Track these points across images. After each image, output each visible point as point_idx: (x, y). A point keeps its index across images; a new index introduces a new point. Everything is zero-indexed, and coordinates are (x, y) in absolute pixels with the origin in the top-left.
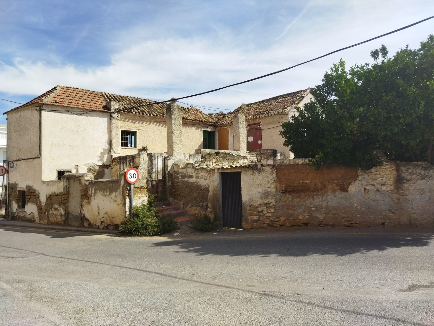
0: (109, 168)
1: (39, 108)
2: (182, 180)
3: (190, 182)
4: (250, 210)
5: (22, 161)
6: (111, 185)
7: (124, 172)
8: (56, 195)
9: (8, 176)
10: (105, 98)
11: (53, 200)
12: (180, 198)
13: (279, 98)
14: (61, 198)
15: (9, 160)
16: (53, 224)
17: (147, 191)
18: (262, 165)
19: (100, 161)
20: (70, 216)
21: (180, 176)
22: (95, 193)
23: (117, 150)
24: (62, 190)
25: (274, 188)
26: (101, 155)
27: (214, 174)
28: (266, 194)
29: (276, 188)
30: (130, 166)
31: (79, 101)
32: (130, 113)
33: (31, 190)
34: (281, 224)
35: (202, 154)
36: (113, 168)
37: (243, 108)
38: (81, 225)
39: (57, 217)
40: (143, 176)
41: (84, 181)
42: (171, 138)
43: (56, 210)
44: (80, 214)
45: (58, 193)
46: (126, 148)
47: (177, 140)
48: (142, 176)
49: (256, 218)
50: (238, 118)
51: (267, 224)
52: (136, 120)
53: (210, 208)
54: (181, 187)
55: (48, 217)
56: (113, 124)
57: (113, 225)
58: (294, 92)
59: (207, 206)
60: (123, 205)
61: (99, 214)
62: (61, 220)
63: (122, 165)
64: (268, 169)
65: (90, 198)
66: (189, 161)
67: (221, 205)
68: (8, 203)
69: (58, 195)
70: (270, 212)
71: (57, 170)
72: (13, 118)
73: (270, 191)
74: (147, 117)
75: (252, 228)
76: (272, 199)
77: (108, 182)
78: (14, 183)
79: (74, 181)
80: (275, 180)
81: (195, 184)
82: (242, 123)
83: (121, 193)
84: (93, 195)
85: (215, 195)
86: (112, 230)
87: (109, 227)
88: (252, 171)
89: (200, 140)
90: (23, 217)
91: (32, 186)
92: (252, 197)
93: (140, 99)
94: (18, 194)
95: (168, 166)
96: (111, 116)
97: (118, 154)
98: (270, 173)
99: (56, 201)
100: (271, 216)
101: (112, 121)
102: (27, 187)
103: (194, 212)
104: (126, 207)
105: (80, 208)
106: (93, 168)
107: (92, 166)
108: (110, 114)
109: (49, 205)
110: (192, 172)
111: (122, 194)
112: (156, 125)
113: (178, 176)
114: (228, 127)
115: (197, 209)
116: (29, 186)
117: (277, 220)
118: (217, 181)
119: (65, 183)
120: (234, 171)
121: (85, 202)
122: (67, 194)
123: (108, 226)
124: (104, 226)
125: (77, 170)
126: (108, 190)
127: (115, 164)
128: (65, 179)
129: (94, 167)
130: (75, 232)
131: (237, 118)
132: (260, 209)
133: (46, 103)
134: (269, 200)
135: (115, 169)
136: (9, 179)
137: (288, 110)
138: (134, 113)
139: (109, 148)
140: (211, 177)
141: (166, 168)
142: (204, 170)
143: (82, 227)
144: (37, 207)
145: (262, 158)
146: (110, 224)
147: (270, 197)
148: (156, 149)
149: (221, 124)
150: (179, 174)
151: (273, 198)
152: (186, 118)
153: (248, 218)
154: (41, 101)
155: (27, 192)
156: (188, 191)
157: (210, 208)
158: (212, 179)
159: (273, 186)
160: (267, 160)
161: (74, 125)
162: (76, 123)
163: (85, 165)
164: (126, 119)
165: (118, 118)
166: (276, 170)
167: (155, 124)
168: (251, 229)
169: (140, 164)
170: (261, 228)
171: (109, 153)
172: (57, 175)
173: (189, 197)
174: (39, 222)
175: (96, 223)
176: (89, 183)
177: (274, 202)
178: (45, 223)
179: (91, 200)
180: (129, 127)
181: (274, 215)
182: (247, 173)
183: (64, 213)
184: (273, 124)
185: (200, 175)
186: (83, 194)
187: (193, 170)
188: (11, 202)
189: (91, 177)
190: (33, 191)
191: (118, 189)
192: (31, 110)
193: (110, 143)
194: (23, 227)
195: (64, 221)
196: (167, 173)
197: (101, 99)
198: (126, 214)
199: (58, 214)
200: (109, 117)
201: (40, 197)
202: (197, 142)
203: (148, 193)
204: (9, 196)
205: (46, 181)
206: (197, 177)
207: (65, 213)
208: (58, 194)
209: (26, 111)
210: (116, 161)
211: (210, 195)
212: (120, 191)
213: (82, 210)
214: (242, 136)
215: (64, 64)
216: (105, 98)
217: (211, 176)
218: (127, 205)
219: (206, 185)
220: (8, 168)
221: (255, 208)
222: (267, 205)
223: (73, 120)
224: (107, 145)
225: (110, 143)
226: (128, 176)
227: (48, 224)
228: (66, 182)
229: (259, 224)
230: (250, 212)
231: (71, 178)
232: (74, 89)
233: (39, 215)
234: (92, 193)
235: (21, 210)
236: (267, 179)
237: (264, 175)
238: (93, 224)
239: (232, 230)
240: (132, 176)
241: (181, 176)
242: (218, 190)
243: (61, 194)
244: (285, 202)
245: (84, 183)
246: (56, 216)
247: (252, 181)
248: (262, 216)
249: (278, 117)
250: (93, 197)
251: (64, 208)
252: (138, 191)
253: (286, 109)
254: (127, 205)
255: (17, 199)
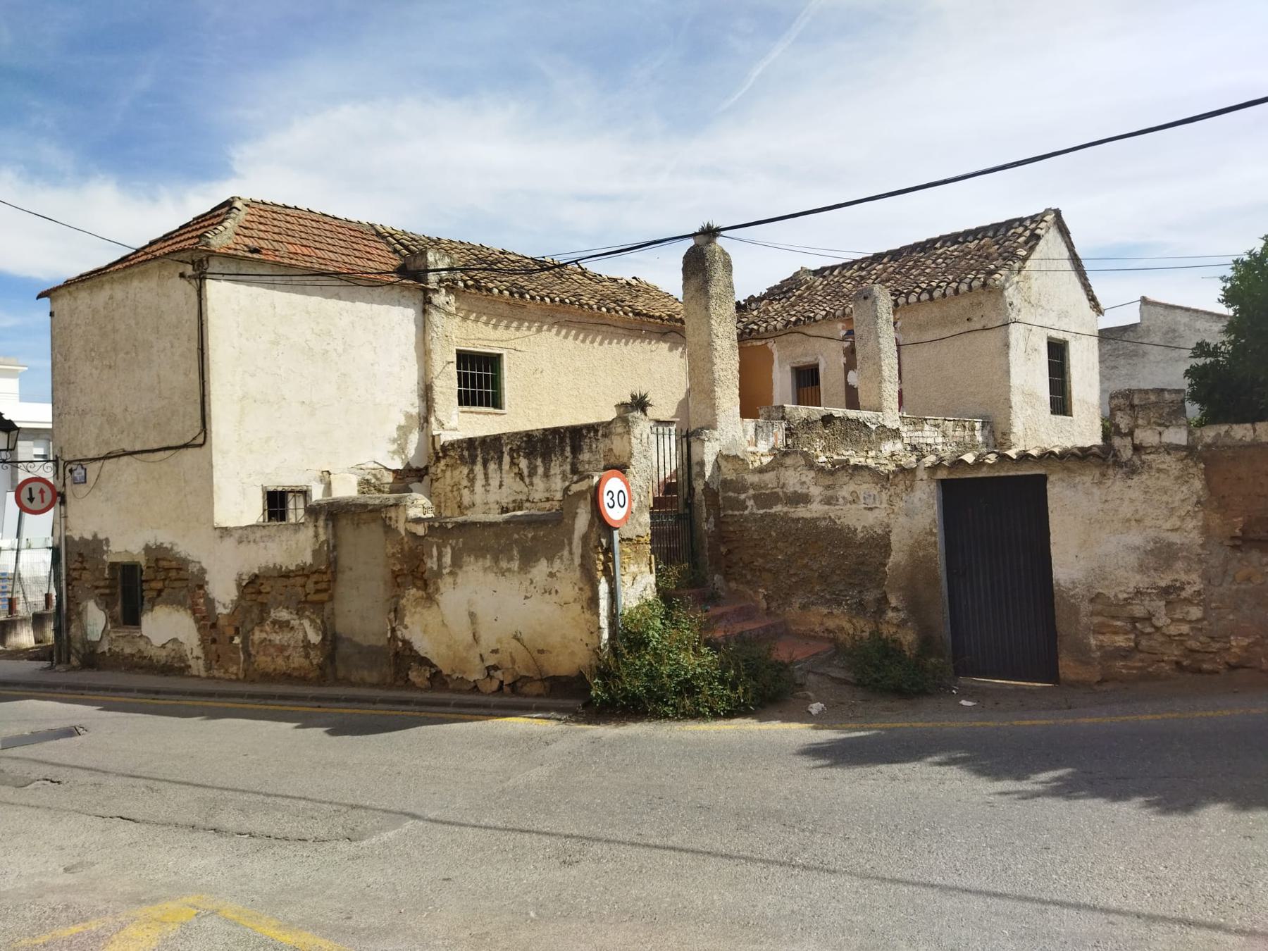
0: (426, 477)
1: (194, 270)
2: (761, 512)
3: (798, 520)
4: (1093, 614)
5: (125, 459)
6: (530, 535)
7: (590, 487)
8: (282, 576)
9: (66, 512)
10: (389, 243)
11: (268, 593)
12: (749, 577)
13: (938, 245)
14: (304, 586)
15: (67, 458)
16: (267, 677)
17: (653, 552)
18: (1137, 449)
19: (396, 457)
20: (343, 649)
21: (750, 499)
22: (457, 563)
23: (449, 417)
24: (308, 559)
25: (1196, 532)
26: (399, 435)
27: (910, 488)
28: (1163, 554)
29: (1206, 530)
30: (517, 471)
31: (317, 251)
32: (485, 293)
33: (164, 559)
34: (1233, 661)
35: (788, 421)
36: (437, 480)
37: (807, 282)
38: (396, 680)
39: (286, 654)
40: (642, 498)
41: (407, 521)
42: (709, 365)
43: (280, 627)
44: (389, 640)
45: (293, 568)
46: (472, 412)
47: (725, 373)
48: (637, 497)
49: (1123, 644)
50: (874, 302)
51: (1172, 661)
52: (501, 317)
53: (895, 609)
54: (755, 537)
55: (248, 655)
56: (435, 329)
57: (541, 680)
58: (992, 225)
59: (883, 601)
60: (589, 605)
61: (476, 638)
62: (308, 662)
63: (478, 468)
64: (1170, 462)
65: (435, 583)
66: (756, 446)
67: (947, 598)
68: (68, 609)
69: (292, 574)
70: (1183, 620)
71: (264, 488)
72: (81, 308)
73: (1178, 542)
74: (531, 306)
75: (1106, 681)
76: (1187, 572)
77: (514, 522)
78: (88, 536)
79: (358, 524)
80: (1198, 502)
81: (823, 523)
82: (884, 317)
83: (577, 561)
84: (445, 571)
85: (918, 564)
86: (538, 696)
87: (522, 687)
88: (1097, 473)
89: (680, 383)
90: (133, 655)
91: (169, 546)
92: (1101, 568)
93: (488, 249)
94: (106, 575)
95: (702, 464)
96: (428, 301)
97: (452, 432)
98: (1177, 478)
99: (282, 598)
100: (1188, 635)
101: (430, 317)
102: (147, 549)
103: (822, 624)
104: (601, 611)
105: (390, 620)
106: (378, 479)
107: (373, 472)
108: (422, 293)
109: (248, 611)
110: (804, 483)
111: (582, 565)
112: (558, 333)
113: (743, 496)
114: (772, 340)
115: (835, 611)
116: (160, 547)
117: (1215, 646)
118: (930, 512)
119: (321, 531)
120: (1012, 473)
121: (411, 597)
122: (329, 571)
123: (519, 684)
124: (502, 682)
125: (328, 487)
126: (515, 553)
127: (447, 466)
128: (322, 518)
129: (379, 476)
130: (390, 707)
131: (869, 301)
132: (1138, 611)
133: (222, 251)
134: (1176, 577)
135: (448, 481)
136: (69, 524)
137: (1003, 277)
138: (496, 291)
139: (424, 411)
140: (896, 500)
141: (695, 469)
142: (863, 473)
143: (400, 688)
144: (197, 621)
145: (1140, 422)
146: (527, 675)
147: (1179, 565)
148: (561, 414)
149: (748, 331)
150: (744, 489)
151: (1195, 566)
152: (645, 312)
153: (1089, 644)
154: (203, 243)
155: (148, 567)
156: (790, 551)
157: (895, 609)
158: (902, 504)
159: (1190, 524)
160: (1160, 429)
161: (313, 329)
162: (318, 323)
163: (351, 470)
164: (470, 311)
165: (449, 308)
166: (1202, 466)
167: (554, 330)
168: (1099, 683)
169: (631, 455)
170: (1145, 677)
171: (422, 429)
172: (264, 506)
173: (792, 572)
174: (203, 674)
175: (465, 672)
176: (431, 528)
177: (1198, 580)
178: (233, 677)
179: (437, 589)
180: (479, 339)
181: (1200, 630)
182: (1077, 480)
183: (320, 638)
184: (945, 327)
185: (845, 492)
186: (401, 570)
187: (812, 474)
188: (78, 604)
189: (425, 510)
190: (174, 564)
191: (562, 549)
192: (156, 278)
193: (426, 393)
194: (157, 692)
195: (320, 667)
196: (703, 487)
197: (378, 245)
198: (600, 637)
199: (292, 643)
200: (420, 305)
201: (207, 583)
202: (674, 390)
203: (656, 559)
204: (68, 584)
205: (236, 528)
206: (828, 501)
207: (323, 639)
208: (292, 571)
209: (136, 283)
210: (452, 453)
211: (897, 565)
212: (571, 553)
213: (401, 628)
214: (887, 361)
215: (84, 175)
216: (389, 243)
217: (897, 495)
218: (604, 604)
219: (872, 527)
220: (64, 485)
221: (1117, 605)
222: (1168, 593)
223: (308, 312)
224: (417, 401)
225: (426, 393)
226: (606, 499)
227: (248, 678)
228: (326, 526)
229: (1140, 664)
230: (1097, 620)
231: (347, 512)
232: (288, 211)
233: (204, 648)
234: (440, 566)
235: (123, 632)
236: (1165, 498)
237: (1149, 483)
238: (448, 676)
239: (1002, 691)
240: (615, 498)
241: (755, 497)
242: (935, 543)
243: (303, 572)
244: (1248, 579)
245: (406, 529)
246: (282, 649)
247: (1100, 506)
248: (1149, 634)
249: (965, 302)
250: (449, 580)
251: (319, 621)
252: (629, 554)
253: (997, 276)
254: (604, 604)
255: (102, 595)
